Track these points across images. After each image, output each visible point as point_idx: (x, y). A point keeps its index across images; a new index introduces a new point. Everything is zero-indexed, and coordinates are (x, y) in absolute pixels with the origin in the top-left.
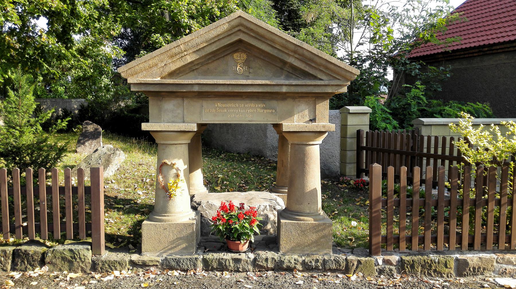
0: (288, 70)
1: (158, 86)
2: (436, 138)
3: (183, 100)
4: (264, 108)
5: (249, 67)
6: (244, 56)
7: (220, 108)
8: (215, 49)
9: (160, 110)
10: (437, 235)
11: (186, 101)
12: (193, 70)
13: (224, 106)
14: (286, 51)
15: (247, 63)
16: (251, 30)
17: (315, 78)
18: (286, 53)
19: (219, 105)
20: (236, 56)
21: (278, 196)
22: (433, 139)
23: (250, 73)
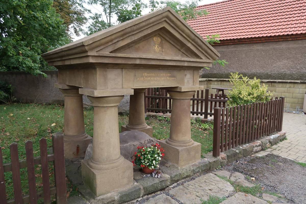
0: (183, 52)
1: (112, 58)
2: (202, 91)
3: (122, 70)
4: (170, 77)
5: (162, 48)
6: (159, 40)
7: (146, 77)
8: (150, 32)
9: (105, 78)
10: (123, 141)
11: (124, 71)
12: (129, 48)
13: (148, 75)
14: (188, 39)
15: (161, 45)
16: (172, 22)
17: (198, 57)
18: (188, 40)
19: (146, 74)
20: (155, 39)
21: (139, 131)
22: (200, 93)
23: (162, 52)
